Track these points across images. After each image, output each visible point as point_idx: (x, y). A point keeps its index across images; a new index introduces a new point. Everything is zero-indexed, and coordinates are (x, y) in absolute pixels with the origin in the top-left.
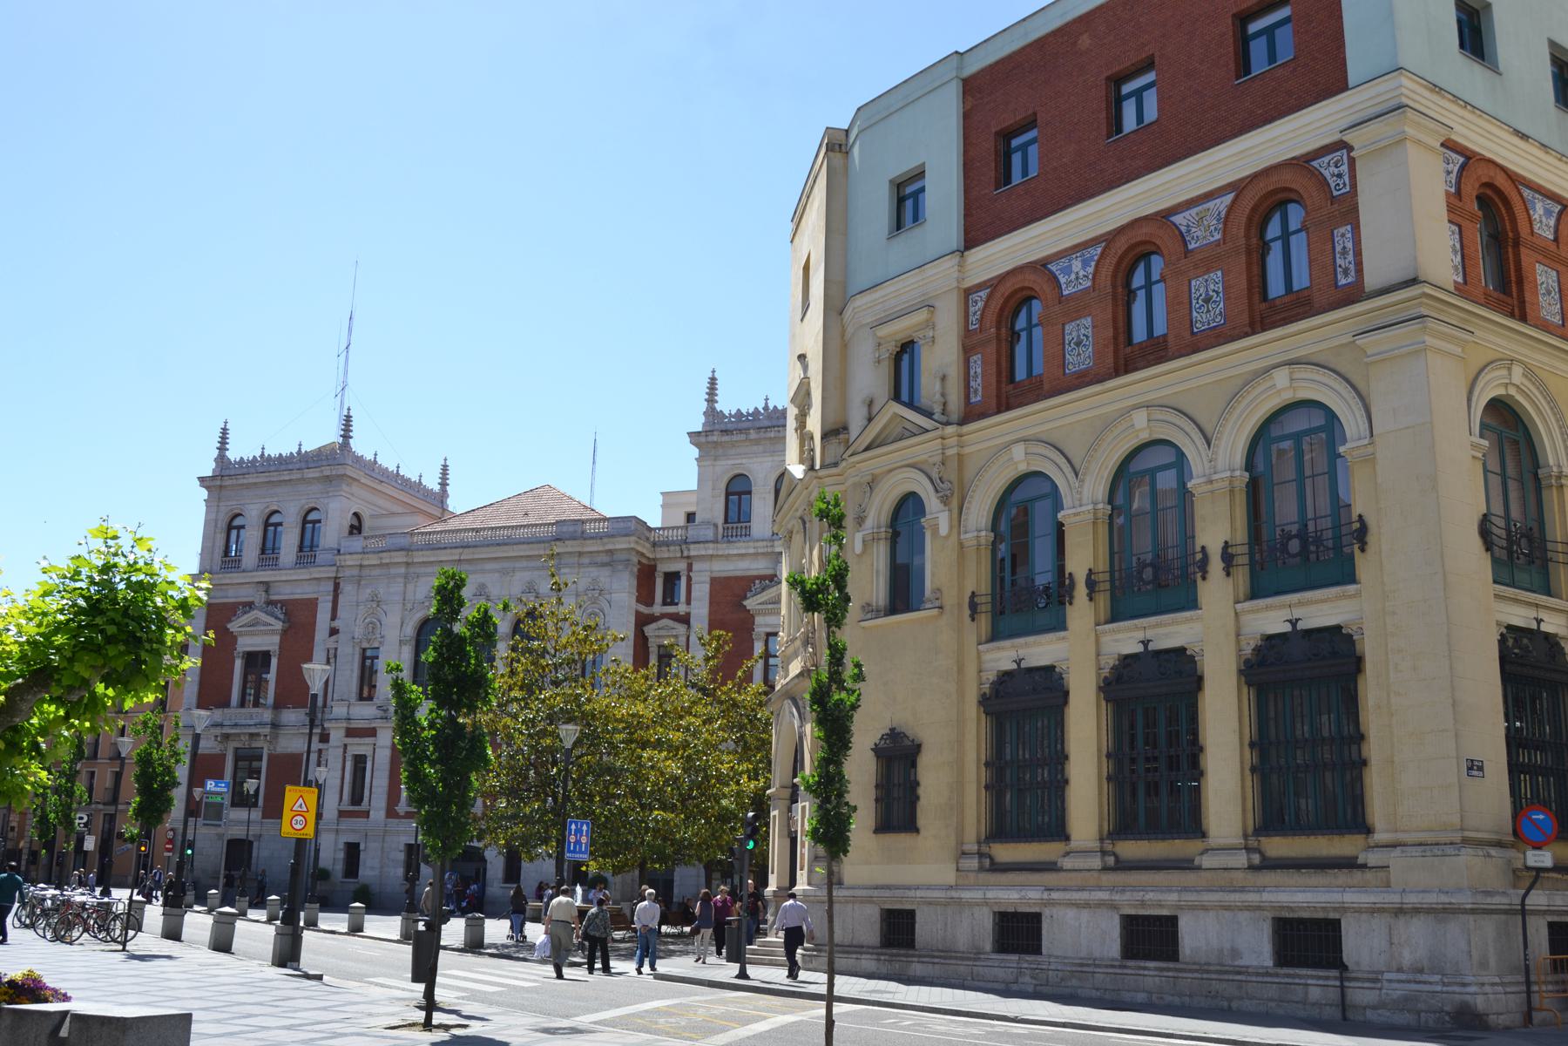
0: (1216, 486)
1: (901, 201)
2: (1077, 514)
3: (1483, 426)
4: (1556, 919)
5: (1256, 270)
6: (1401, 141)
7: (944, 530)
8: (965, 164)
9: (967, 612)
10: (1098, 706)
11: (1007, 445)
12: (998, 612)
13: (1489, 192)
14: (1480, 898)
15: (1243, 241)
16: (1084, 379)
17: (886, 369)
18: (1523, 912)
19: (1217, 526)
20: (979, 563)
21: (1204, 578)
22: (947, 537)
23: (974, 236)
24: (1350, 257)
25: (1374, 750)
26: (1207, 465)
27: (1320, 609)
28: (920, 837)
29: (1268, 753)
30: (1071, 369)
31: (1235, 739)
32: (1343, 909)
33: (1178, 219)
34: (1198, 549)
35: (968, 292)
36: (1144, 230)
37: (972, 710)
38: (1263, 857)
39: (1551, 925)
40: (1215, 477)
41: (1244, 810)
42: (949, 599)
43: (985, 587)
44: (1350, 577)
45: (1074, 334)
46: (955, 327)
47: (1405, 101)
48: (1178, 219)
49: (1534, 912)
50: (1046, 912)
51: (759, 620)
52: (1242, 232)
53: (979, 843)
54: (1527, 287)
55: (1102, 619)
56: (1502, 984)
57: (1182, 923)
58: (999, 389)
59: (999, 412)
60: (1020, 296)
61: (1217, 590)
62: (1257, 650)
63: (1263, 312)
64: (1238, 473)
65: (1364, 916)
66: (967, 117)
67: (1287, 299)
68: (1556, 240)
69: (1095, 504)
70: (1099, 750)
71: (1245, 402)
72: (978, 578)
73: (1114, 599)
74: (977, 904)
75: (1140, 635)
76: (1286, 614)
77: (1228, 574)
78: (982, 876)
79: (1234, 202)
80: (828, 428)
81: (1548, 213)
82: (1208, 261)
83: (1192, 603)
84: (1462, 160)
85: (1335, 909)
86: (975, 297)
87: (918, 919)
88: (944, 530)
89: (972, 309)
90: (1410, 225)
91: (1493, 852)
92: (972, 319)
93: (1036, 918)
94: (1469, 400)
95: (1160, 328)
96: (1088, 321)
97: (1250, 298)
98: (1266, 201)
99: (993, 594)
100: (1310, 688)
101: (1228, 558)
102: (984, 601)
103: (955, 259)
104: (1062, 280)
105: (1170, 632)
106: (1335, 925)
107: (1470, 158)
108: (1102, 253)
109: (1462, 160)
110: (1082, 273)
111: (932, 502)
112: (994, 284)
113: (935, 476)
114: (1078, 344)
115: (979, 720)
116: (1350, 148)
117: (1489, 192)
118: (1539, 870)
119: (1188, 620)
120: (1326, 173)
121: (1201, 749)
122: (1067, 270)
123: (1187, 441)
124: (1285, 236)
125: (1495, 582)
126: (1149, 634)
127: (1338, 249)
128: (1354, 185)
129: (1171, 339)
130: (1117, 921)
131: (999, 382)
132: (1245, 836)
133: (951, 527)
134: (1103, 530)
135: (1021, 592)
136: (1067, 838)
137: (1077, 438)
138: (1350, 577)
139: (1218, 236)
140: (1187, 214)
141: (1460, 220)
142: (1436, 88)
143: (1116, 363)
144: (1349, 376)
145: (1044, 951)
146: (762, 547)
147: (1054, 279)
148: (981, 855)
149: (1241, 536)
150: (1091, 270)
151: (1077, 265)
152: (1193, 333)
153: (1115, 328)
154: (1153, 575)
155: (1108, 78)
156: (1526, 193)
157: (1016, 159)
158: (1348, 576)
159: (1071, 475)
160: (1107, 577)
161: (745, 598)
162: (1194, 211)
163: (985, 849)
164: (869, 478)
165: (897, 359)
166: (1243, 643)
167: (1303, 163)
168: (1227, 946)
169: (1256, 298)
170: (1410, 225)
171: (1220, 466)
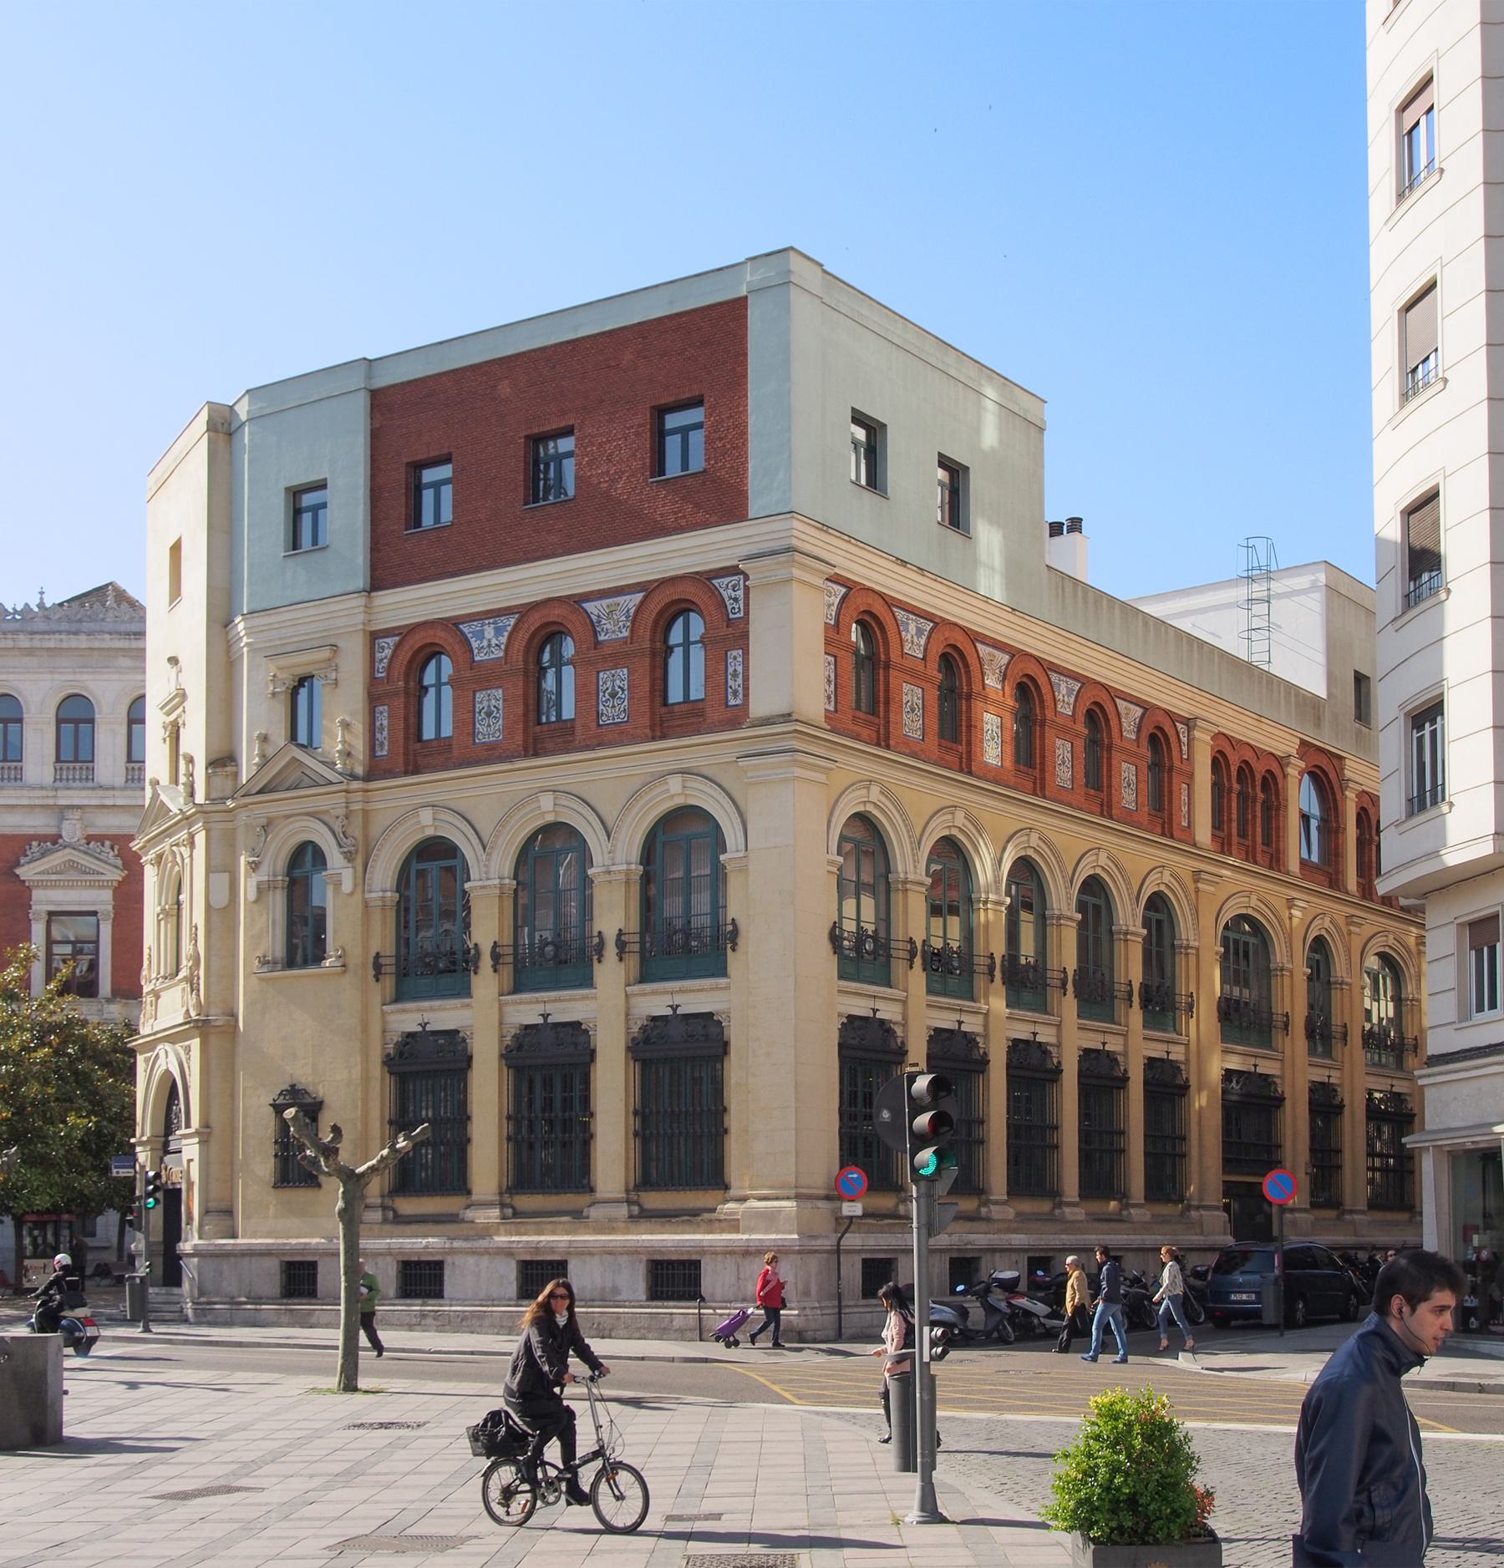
0: (613, 877)
1: (297, 512)
2: (483, 887)
3: (843, 838)
4: (869, 1256)
5: (659, 673)
6: (789, 580)
7: (347, 886)
8: (372, 490)
9: (372, 972)
10: (500, 1070)
11: (415, 808)
12: (402, 974)
13: (867, 618)
14: (806, 1242)
15: (647, 645)
16: (492, 754)
17: (281, 710)
18: (838, 1251)
19: (613, 914)
20: (384, 923)
21: (599, 961)
22: (352, 894)
23: (379, 580)
24: (740, 680)
25: (733, 1121)
26: (606, 855)
27: (693, 997)
28: (322, 1192)
29: (649, 1125)
30: (480, 739)
31: (622, 1106)
32: (703, 1250)
33: (590, 607)
34: (729, 921)
35: (374, 636)
36: (557, 612)
37: (376, 1069)
38: (642, 1210)
39: (865, 1261)
40: (614, 868)
41: (627, 1169)
42: (355, 959)
43: (390, 949)
44: (722, 972)
45: (485, 703)
46: (361, 673)
47: (795, 542)
48: (590, 607)
49: (849, 1252)
50: (449, 1260)
51: (37, 894)
52: (648, 636)
53: (382, 1196)
54: (893, 707)
55: (506, 989)
56: (821, 1308)
57: (570, 1267)
58: (406, 746)
59: (406, 773)
60: (428, 650)
61: (610, 973)
62: (643, 1028)
63: (664, 719)
64: (633, 867)
65: (720, 1258)
66: (375, 436)
67: (684, 707)
68: (924, 659)
69: (501, 878)
70: (500, 1113)
71: (643, 802)
72: (383, 939)
73: (517, 971)
74: (381, 1254)
75: (540, 1008)
76: (667, 1000)
77: (621, 959)
78: (387, 1227)
79: (642, 602)
80: (215, 756)
81: (919, 632)
82: (615, 658)
83: (587, 981)
84: (844, 590)
85: (697, 1252)
86: (382, 642)
87: (320, 1269)
88: (347, 886)
89: (378, 656)
90: (791, 664)
91: (820, 1204)
92: (381, 666)
93: (439, 1265)
94: (829, 822)
95: (697, 693)
96: (499, 693)
97: (652, 701)
98: (670, 604)
99: (398, 956)
100: (685, 1074)
101: (621, 945)
102: (389, 963)
103: (361, 601)
104: (475, 645)
105: (565, 1006)
106: (695, 1265)
107: (850, 586)
108: (516, 625)
109: (844, 590)
110: (494, 642)
111: (334, 858)
112: (405, 633)
113: (338, 830)
114: (489, 714)
115: (382, 1079)
116: (747, 578)
117: (867, 618)
118: (851, 1218)
119: (584, 998)
120: (724, 594)
121: (592, 1136)
122: (480, 635)
123: (590, 830)
124: (687, 644)
125: (841, 977)
126: (549, 1008)
127: (730, 670)
128: (747, 613)
129: (578, 725)
130: (513, 1265)
131: (406, 738)
132: (627, 1191)
133: (355, 886)
134: (509, 904)
135: (427, 957)
136: (469, 1193)
137: (487, 811)
138: (722, 972)
139: (626, 634)
140: (597, 603)
141: (835, 651)
142: (824, 527)
143: (525, 741)
144: (732, 792)
145: (446, 1294)
146: (37, 798)
147: (715, 594)
148: (384, 1208)
149: (634, 925)
150: (504, 640)
151: (489, 632)
152: (599, 725)
153: (526, 705)
154: (558, 959)
155: (526, 437)
156: (900, 614)
157: (673, 444)
158: (719, 969)
159: (479, 847)
160: (510, 950)
161: (18, 865)
162: (605, 602)
163: (388, 1202)
164: (264, 821)
165: (294, 693)
166: (631, 1023)
167: (705, 579)
168: (609, 1284)
169: (658, 700)
170: (791, 664)
171: (617, 860)
